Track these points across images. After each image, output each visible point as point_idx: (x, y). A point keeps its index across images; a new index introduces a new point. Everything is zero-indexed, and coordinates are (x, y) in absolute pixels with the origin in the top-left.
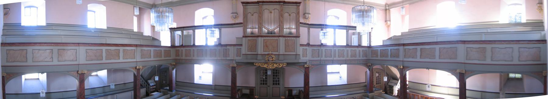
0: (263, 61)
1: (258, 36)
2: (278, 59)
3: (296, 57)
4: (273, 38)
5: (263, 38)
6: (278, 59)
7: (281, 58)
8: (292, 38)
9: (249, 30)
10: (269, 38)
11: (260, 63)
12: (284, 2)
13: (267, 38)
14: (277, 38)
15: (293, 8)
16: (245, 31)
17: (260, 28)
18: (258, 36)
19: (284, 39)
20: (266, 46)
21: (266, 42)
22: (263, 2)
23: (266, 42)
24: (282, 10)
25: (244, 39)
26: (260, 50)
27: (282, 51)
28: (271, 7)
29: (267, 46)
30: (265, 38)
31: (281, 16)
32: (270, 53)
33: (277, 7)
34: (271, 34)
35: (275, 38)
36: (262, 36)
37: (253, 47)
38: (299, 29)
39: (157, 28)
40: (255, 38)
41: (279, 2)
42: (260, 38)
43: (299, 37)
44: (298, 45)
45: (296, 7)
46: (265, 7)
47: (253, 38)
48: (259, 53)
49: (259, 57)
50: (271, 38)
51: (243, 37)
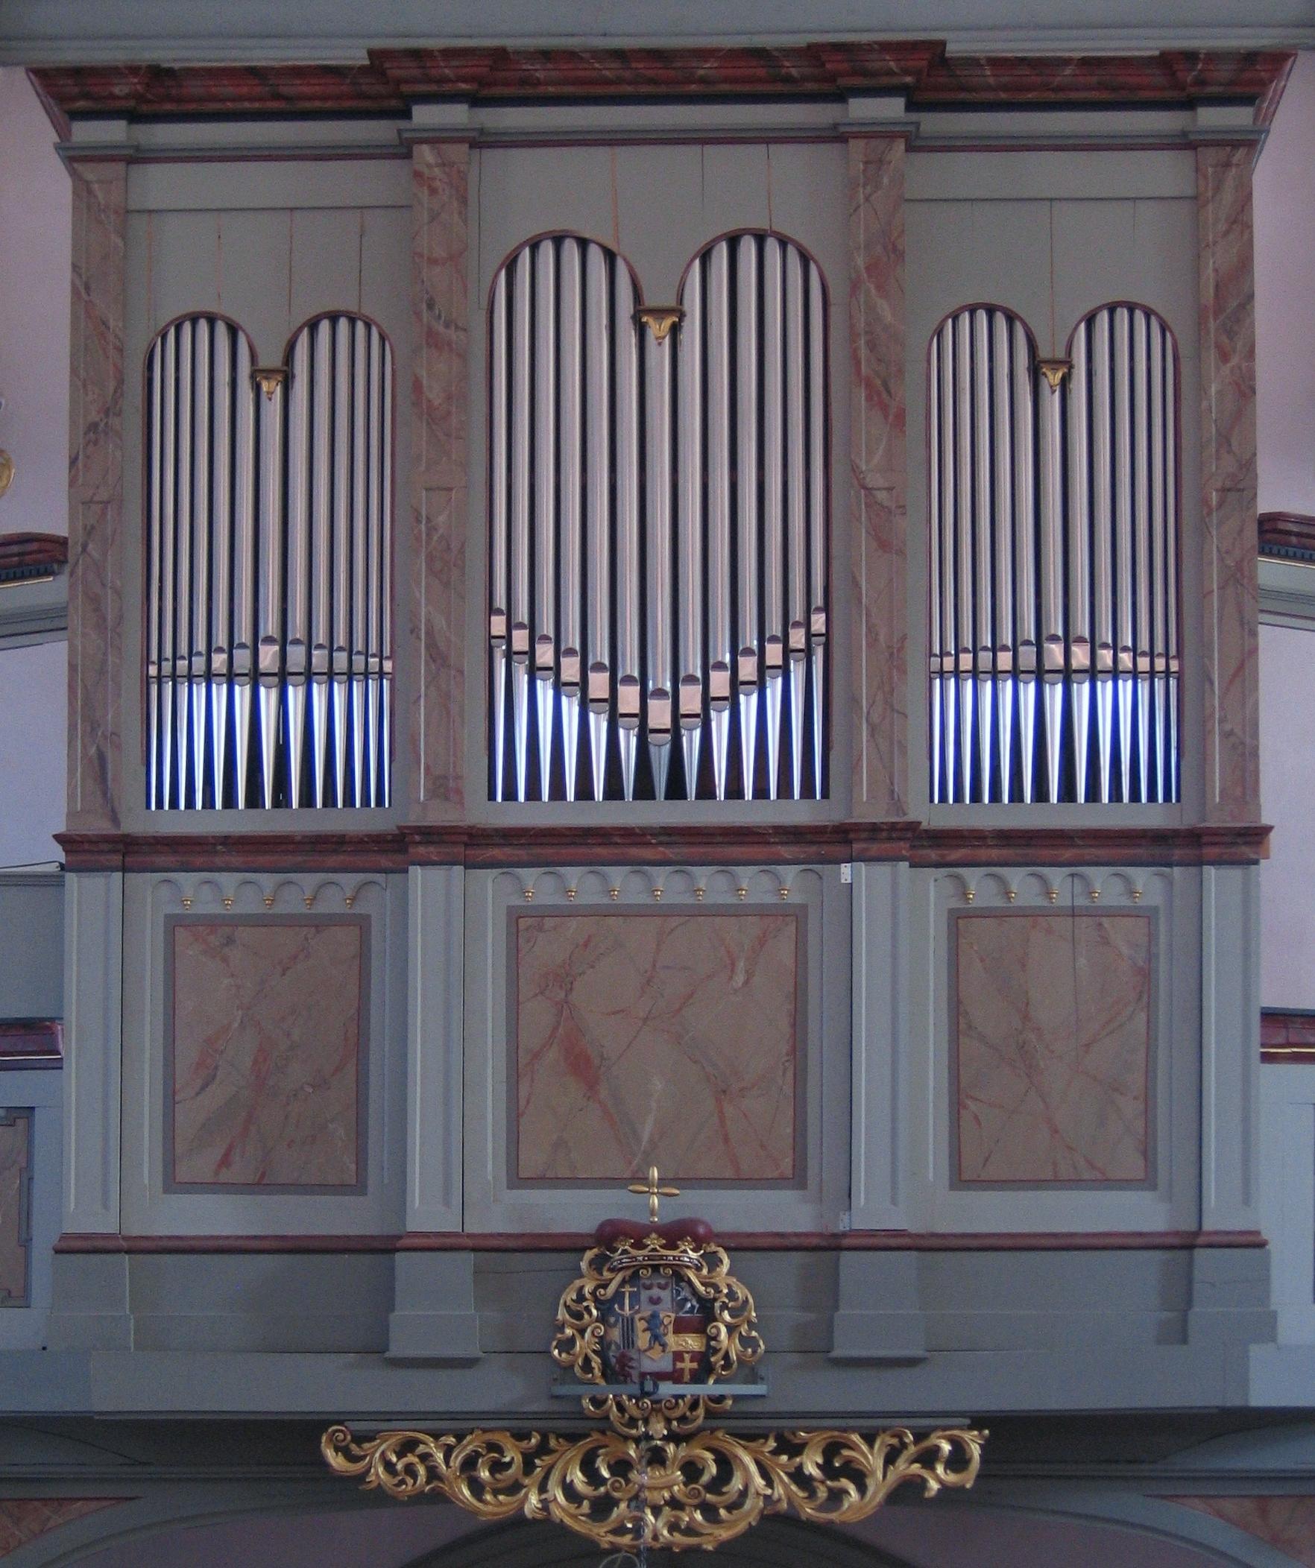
0: (499, 1388)
1: (395, 849)
2: (817, 1349)
3: (1181, 1296)
4: (709, 884)
5: (492, 890)
6: (817, 1349)
7: (876, 1306)
8: (1105, 884)
9: (209, 718)
10: (623, 884)
11: (454, 1425)
12: (933, 78)
13: (580, 884)
14: (791, 882)
15: (1089, 213)
16: (104, 737)
17: (854, 639)
18: (395, 849)
19: (931, 891)
20: (561, 1055)
21: (562, 979)
22: (494, 76)
23: (562, 979)
24: (885, 260)
25: (91, 894)
26: (452, 1158)
27: (896, 1169)
28: (661, 190)
29: (583, 1066)
30: (538, 886)
31: (867, 381)
32: (656, 1205)
33: (782, 181)
34: (659, 817)
35: (753, 884)
36: (472, 846)
37: (302, 1084)
38: (1244, 670)
39: (715, 1444)
40: (334, 891)
41: (826, 72)
42: (427, 885)
43: (1244, 843)
44: (1227, 1034)
45: (1165, 173)
46: (533, 185)
47: (300, 892)
48: (426, 1211)
49: (437, 1306)
50: (667, 885)
51: (83, 850)
